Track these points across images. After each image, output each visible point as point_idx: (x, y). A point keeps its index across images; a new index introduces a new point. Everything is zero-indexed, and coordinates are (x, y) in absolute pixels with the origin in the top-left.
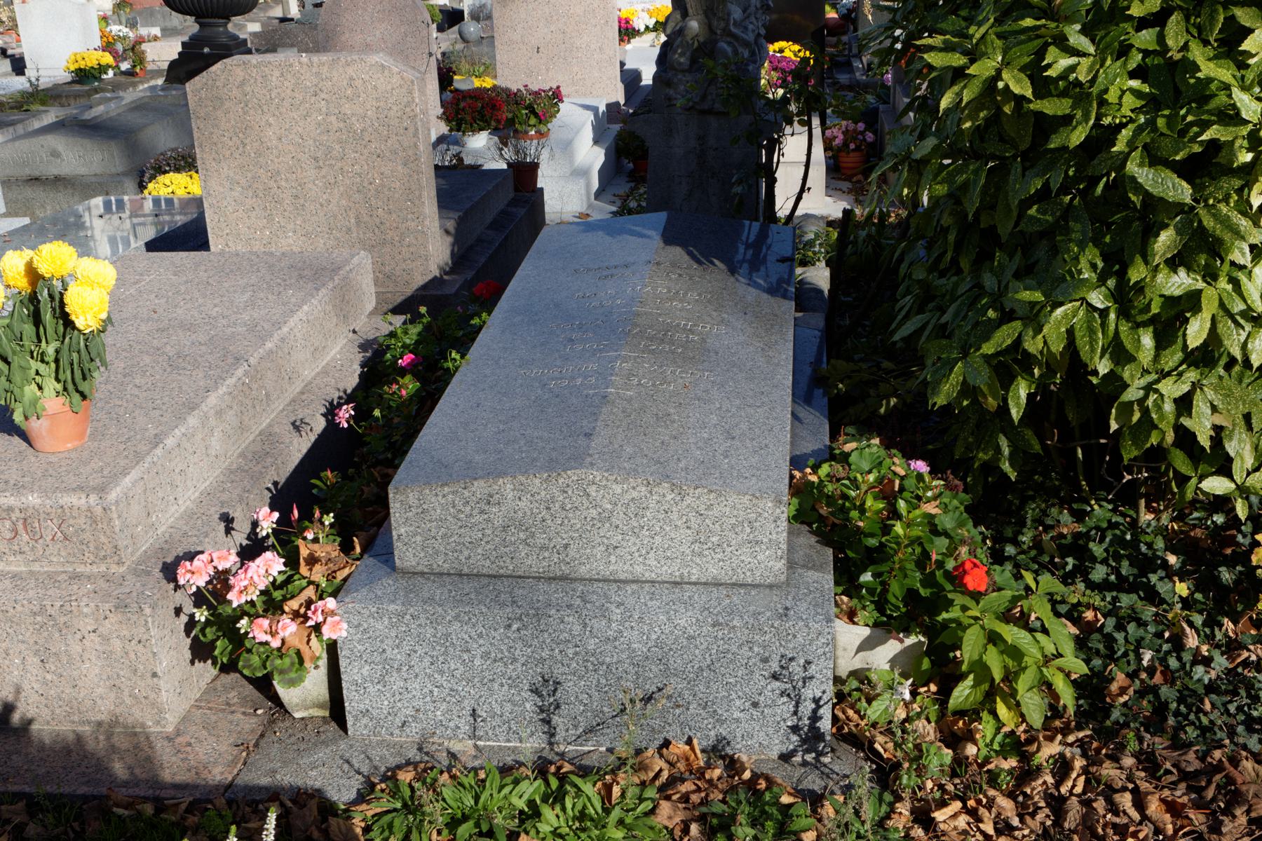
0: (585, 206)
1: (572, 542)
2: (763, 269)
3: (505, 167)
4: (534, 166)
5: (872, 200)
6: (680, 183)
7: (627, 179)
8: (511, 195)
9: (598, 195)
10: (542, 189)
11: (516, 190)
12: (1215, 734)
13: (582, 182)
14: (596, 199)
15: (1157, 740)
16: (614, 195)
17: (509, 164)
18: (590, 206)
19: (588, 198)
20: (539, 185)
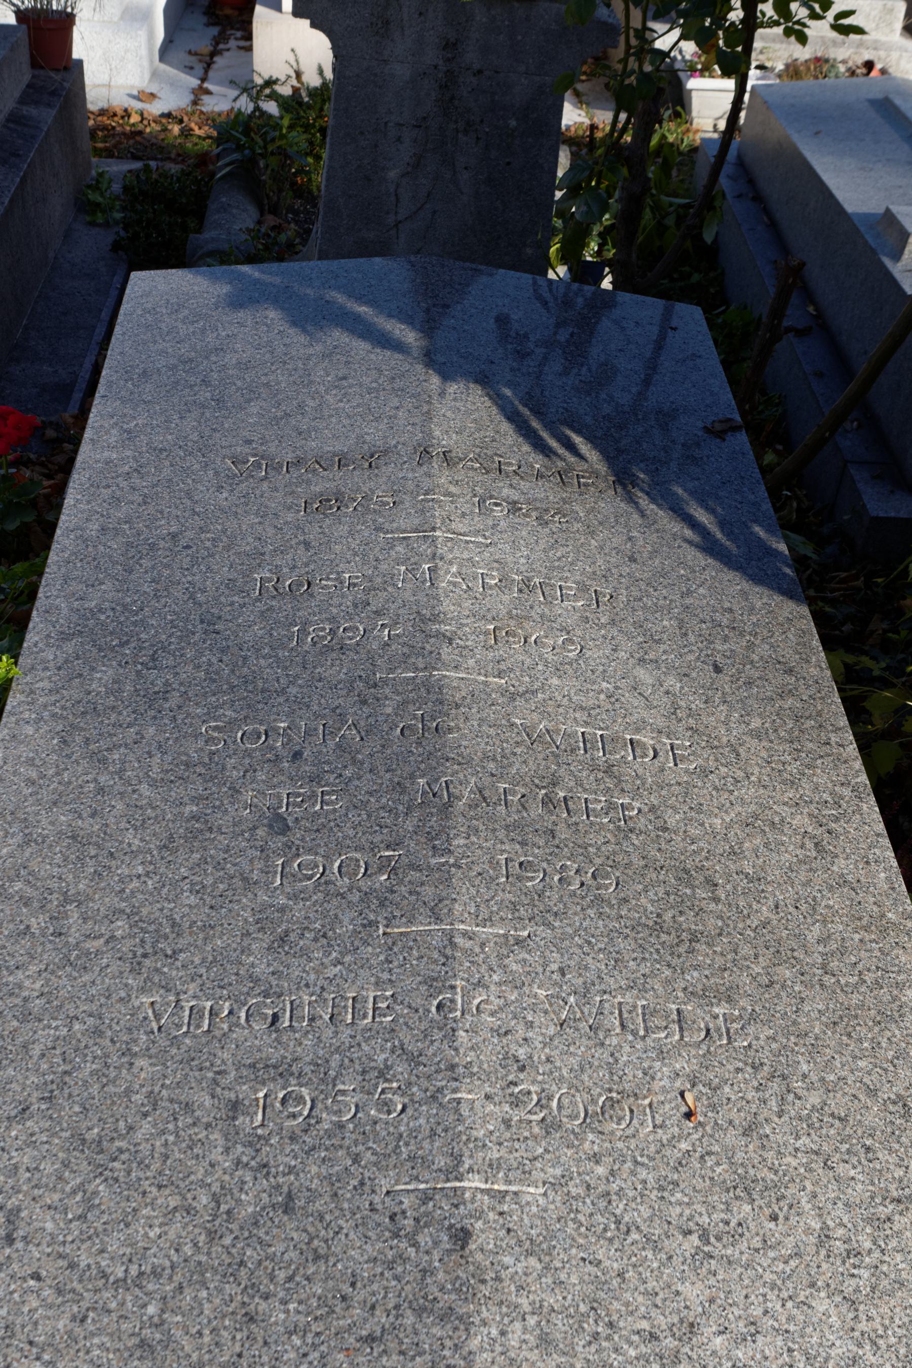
0: (147, 76)
1: (450, 1333)
2: (790, 562)
3: (11, 20)
4: (66, 21)
5: (644, 229)
6: (399, 139)
7: (204, 19)
8: (26, 78)
9: (165, 52)
10: (80, 63)
11: (34, 65)
12: (270, 571)
13: (143, 34)
14: (161, 59)
15: (29, 1124)
16: (190, 52)
17: (21, 15)
18: (154, 74)
19: (151, 62)
20: (75, 55)
